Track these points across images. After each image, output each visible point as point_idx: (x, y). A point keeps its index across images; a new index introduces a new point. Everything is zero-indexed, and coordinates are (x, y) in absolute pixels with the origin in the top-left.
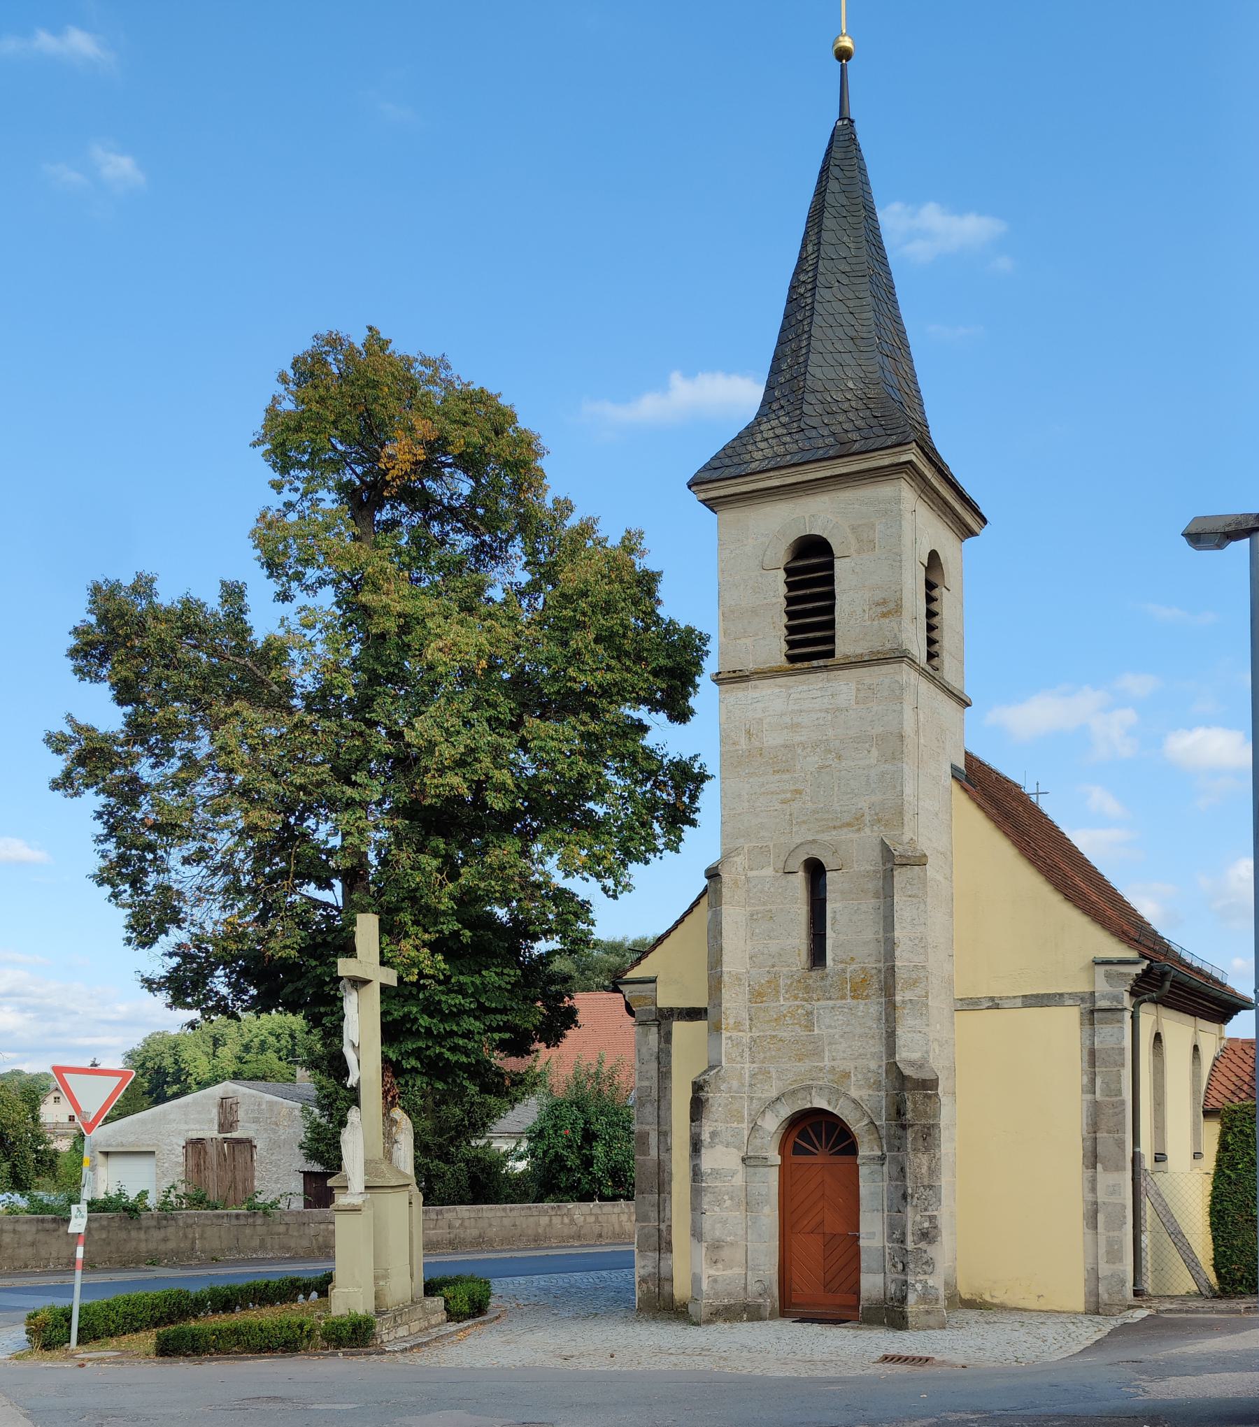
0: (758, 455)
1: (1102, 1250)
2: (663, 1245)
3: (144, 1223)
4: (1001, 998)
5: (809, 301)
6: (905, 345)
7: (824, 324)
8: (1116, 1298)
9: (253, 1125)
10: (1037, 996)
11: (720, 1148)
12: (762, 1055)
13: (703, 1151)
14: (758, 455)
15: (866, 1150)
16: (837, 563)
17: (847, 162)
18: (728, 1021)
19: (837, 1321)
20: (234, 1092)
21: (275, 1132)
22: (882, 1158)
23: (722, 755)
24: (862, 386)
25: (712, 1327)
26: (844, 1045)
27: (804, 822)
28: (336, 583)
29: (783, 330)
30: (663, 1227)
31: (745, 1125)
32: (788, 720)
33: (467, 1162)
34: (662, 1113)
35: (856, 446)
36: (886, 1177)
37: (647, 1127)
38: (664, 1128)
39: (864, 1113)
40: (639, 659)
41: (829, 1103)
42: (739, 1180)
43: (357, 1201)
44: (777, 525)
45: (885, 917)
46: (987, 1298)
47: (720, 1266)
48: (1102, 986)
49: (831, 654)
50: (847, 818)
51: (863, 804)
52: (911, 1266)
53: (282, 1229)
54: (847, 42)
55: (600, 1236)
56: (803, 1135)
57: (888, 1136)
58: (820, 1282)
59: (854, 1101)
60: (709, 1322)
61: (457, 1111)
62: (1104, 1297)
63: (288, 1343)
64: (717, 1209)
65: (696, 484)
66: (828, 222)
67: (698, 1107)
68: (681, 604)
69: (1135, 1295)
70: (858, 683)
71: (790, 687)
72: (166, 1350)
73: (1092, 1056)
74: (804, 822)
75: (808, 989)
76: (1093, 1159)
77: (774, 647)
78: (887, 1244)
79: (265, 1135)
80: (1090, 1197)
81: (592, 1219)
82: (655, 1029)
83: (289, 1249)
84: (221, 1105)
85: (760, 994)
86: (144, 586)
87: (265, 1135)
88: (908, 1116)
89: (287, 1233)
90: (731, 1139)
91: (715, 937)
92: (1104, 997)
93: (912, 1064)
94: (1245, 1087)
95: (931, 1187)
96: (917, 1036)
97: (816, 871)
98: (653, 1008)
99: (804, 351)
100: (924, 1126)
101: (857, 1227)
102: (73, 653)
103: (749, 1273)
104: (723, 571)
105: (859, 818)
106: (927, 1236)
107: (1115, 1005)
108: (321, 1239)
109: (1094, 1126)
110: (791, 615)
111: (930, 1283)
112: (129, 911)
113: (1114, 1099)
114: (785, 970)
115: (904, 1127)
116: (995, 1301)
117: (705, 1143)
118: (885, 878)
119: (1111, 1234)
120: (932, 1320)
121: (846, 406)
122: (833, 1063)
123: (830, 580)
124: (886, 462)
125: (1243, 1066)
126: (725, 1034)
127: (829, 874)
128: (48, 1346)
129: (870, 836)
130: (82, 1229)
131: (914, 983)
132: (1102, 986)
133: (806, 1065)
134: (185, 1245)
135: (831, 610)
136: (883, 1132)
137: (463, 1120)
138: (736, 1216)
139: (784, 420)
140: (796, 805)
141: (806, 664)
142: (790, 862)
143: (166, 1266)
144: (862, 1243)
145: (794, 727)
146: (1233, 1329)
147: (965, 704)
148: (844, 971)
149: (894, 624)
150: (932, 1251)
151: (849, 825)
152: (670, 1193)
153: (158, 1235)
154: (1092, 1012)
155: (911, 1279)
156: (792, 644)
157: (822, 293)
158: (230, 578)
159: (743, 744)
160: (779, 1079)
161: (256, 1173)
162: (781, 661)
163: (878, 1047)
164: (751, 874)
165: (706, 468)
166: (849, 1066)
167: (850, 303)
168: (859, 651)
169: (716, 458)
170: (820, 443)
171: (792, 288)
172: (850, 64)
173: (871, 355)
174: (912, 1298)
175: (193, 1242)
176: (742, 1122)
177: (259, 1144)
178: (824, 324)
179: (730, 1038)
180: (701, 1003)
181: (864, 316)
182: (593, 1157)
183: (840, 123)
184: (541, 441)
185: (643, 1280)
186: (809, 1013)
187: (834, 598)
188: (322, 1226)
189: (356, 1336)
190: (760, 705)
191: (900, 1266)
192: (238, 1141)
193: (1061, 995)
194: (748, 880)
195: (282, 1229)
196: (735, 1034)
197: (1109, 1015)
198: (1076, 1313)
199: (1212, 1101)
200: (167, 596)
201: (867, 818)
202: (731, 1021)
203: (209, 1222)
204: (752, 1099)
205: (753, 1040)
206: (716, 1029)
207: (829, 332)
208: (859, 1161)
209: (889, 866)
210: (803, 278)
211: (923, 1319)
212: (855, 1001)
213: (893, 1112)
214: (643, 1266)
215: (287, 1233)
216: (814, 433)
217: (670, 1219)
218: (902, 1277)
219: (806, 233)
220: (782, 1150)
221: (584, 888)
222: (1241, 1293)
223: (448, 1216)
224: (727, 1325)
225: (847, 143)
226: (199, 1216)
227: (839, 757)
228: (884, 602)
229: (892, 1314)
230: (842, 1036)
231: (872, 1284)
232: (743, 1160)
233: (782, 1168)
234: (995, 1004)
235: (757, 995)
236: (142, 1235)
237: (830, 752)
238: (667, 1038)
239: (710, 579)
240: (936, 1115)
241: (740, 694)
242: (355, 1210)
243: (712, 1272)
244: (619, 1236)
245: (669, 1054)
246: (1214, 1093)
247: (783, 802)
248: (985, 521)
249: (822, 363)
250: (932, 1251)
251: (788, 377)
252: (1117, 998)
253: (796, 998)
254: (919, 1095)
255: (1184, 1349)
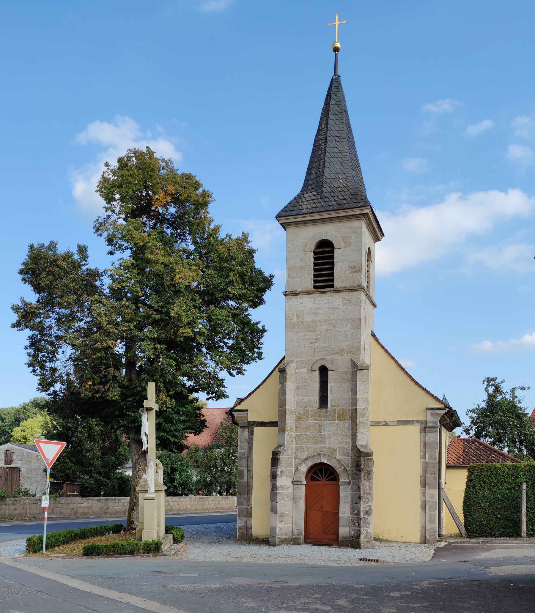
0: (305, 207)
1: (427, 519)
2: (249, 514)
3: (8, 502)
4: (389, 421)
5: (323, 147)
6: (359, 166)
7: (330, 156)
8: (433, 537)
9: (20, 462)
10: (403, 421)
11: (284, 477)
12: (300, 442)
13: (278, 478)
14: (305, 207)
15: (343, 479)
16: (336, 251)
17: (338, 93)
18: (288, 428)
19: (330, 545)
20: (12, 448)
21: (30, 465)
22: (349, 483)
23: (286, 324)
24: (345, 182)
25: (280, 547)
26: (334, 438)
27: (320, 351)
28: (131, 249)
29: (312, 157)
30: (249, 507)
31: (293, 469)
32: (314, 311)
33: (118, 479)
34: (249, 463)
35: (346, 206)
36: (350, 489)
37: (243, 468)
38: (250, 469)
39: (342, 465)
40: (251, 284)
41: (328, 461)
42: (290, 490)
43: (153, 496)
44: (311, 235)
45: (352, 390)
46: (381, 537)
47: (283, 523)
48: (429, 418)
49: (332, 286)
50: (337, 351)
51: (344, 345)
52: (362, 524)
53: (60, 505)
54: (338, 45)
55: (179, 510)
56: (315, 473)
57: (352, 474)
58: (322, 529)
59: (338, 460)
60: (279, 545)
61: (113, 458)
62: (428, 537)
63: (131, 552)
64: (282, 501)
65: (279, 217)
66: (331, 116)
67: (275, 461)
68: (262, 263)
69: (439, 536)
70: (343, 298)
71: (315, 298)
72: (89, 552)
73: (425, 445)
74: (320, 351)
75: (320, 416)
76: (424, 484)
77: (308, 282)
78: (350, 516)
79: (26, 466)
80: (423, 499)
81: (176, 503)
82: (247, 430)
83: (63, 514)
84: (6, 453)
85: (300, 418)
86: (53, 246)
87: (26, 466)
88: (362, 467)
89: (62, 507)
90: (288, 474)
91: (282, 395)
92: (430, 422)
93: (362, 446)
94: (462, 457)
95: (369, 494)
96: (364, 436)
97: (324, 371)
98: (246, 421)
99: (322, 166)
100: (368, 470)
101: (338, 508)
102: (21, 272)
103: (294, 526)
104: (288, 251)
105: (342, 350)
106: (367, 513)
107: (434, 425)
108: (75, 510)
109: (425, 472)
110: (315, 270)
111: (369, 531)
112: (39, 378)
113: (433, 461)
114: (311, 409)
115: (360, 471)
116: (384, 538)
117: (278, 476)
118: (353, 374)
119: (431, 513)
120: (369, 545)
121: (339, 189)
122: (330, 445)
123: (332, 257)
124: (358, 213)
125: (460, 449)
126: (287, 433)
127: (329, 372)
128: (35, 552)
129: (347, 358)
130: (47, 505)
131: (363, 415)
132: (429, 418)
133: (319, 445)
134: (23, 511)
135: (332, 269)
136: (350, 473)
137: (115, 462)
138: (289, 504)
139: (314, 193)
140: (316, 345)
141: (322, 290)
142: (314, 366)
143: (16, 520)
144: (340, 515)
145: (316, 314)
146: (487, 549)
147: (375, 306)
148: (335, 410)
149: (358, 276)
150: (370, 519)
151: (338, 353)
152: (252, 494)
153: (13, 507)
154: (425, 428)
155: (362, 529)
156: (315, 282)
157: (329, 144)
158: (82, 243)
159: (295, 320)
160: (307, 451)
161: (21, 482)
162: (311, 288)
163: (349, 440)
164: (297, 371)
165: (283, 211)
166: (336, 446)
167: (340, 149)
168: (344, 286)
169: (286, 207)
170: (330, 204)
171: (315, 141)
172: (339, 54)
173: (348, 170)
174: (362, 536)
175: (26, 510)
176: (292, 467)
177: (23, 470)
178: (330, 156)
179: (288, 434)
180: (276, 420)
181: (346, 154)
182: (175, 479)
183: (334, 77)
184: (213, 196)
185: (240, 528)
186: (320, 426)
187: (334, 264)
188: (75, 505)
189: (154, 548)
190: (302, 305)
191: (357, 524)
192: (13, 468)
193: (413, 421)
194: (296, 373)
195: (60, 505)
196: (290, 433)
197: (432, 429)
198: (416, 543)
199: (450, 462)
200: (61, 250)
201: (346, 351)
202: (289, 428)
203: (32, 502)
204: (296, 458)
205: (297, 436)
206: (282, 430)
207: (332, 159)
208: (340, 484)
209: (355, 370)
210: (320, 137)
211: (366, 544)
212: (339, 422)
213: (355, 465)
214: (239, 523)
215: (62, 507)
216: (327, 200)
217: (252, 505)
218: (358, 528)
219: (321, 119)
220: (306, 479)
221: (223, 374)
222: (476, 536)
223: (123, 501)
224: (286, 546)
225: (338, 85)
226: (29, 500)
227: (335, 327)
228: (355, 267)
229: (354, 542)
230: (334, 435)
231: (344, 531)
232: (292, 482)
233: (306, 486)
234: (386, 424)
235: (299, 418)
236: (7, 507)
237: (331, 324)
238: (251, 433)
239: (276, 252)
240: (372, 467)
241: (294, 300)
242: (152, 499)
243: (280, 526)
244: (186, 510)
245: (252, 440)
246: (450, 459)
247: (311, 343)
248: (383, 235)
249: (330, 172)
250: (370, 519)
251: (315, 176)
252: (435, 423)
253: (315, 420)
254: (366, 459)
255: (475, 557)
